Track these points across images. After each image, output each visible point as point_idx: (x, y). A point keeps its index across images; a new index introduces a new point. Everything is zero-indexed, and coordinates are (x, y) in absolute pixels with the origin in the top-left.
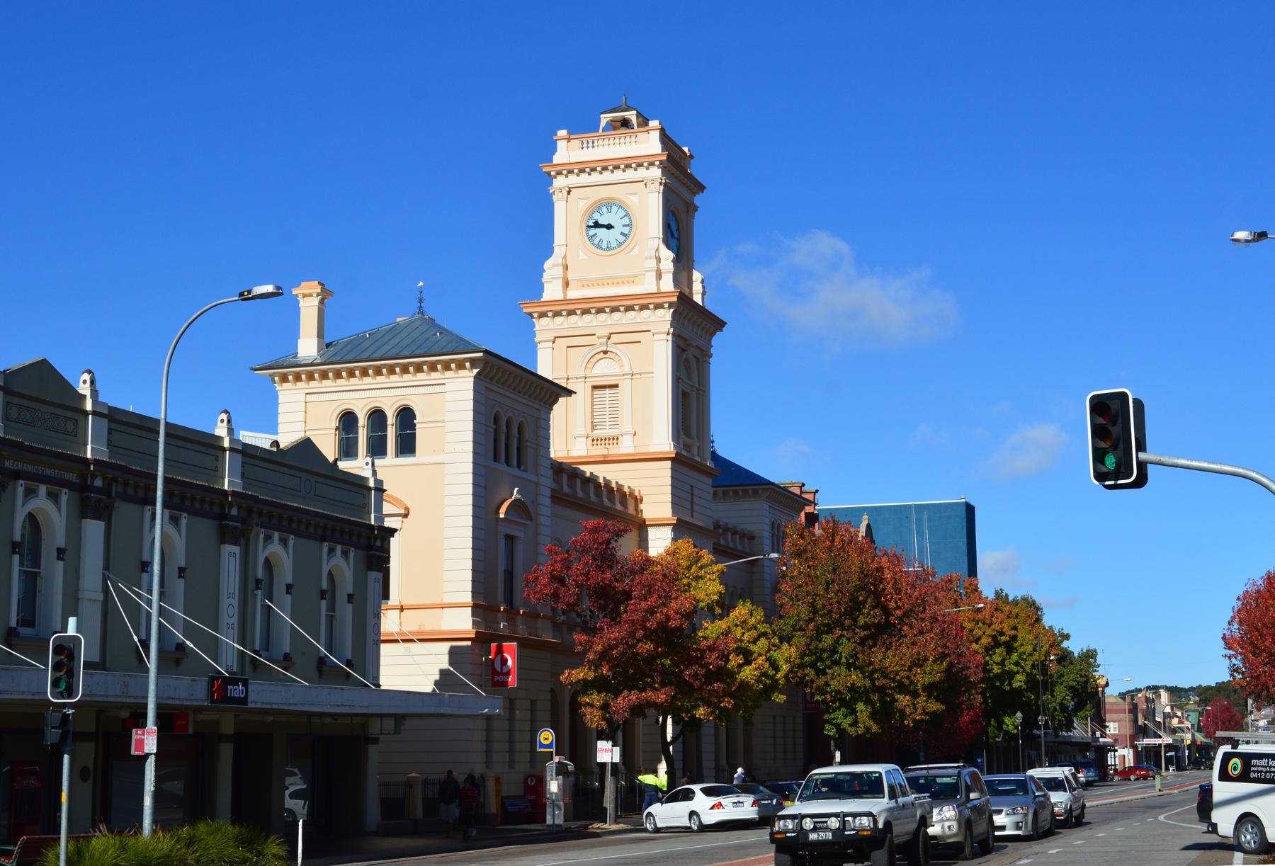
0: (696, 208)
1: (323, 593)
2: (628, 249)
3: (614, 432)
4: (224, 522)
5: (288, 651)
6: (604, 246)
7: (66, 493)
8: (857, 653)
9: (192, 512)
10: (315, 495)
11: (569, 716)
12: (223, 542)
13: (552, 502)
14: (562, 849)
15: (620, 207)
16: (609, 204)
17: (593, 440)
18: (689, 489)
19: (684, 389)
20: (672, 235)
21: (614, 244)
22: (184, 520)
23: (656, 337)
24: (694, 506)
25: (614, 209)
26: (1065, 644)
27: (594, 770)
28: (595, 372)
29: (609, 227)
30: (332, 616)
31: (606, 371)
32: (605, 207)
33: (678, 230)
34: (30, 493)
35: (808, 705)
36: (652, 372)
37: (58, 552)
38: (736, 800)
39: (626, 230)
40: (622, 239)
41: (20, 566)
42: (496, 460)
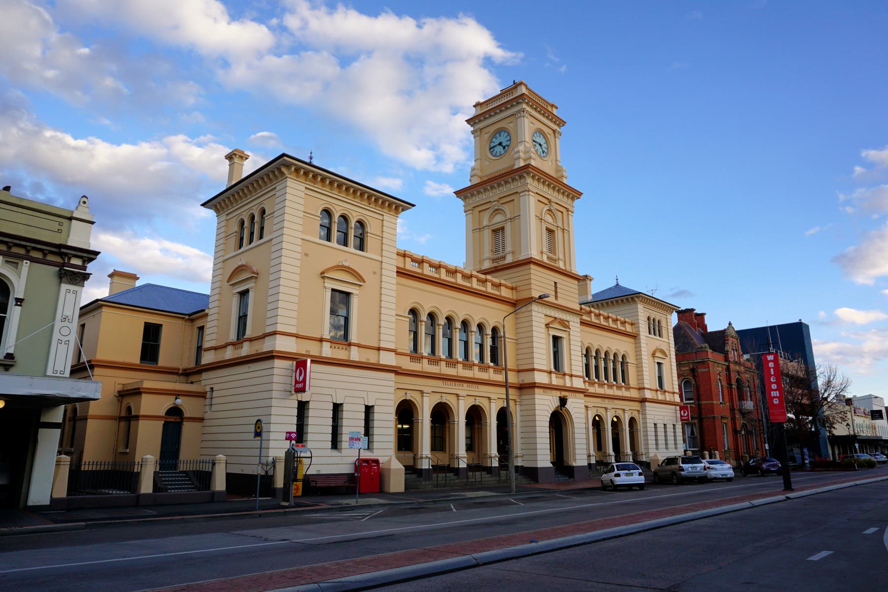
11: (629, 429)
13: (397, 275)
15: (505, 132)
17: (493, 261)
19: (547, 226)
23: (521, 194)
25: (502, 133)
27: (629, 454)
35: (683, 418)
38: (158, 462)
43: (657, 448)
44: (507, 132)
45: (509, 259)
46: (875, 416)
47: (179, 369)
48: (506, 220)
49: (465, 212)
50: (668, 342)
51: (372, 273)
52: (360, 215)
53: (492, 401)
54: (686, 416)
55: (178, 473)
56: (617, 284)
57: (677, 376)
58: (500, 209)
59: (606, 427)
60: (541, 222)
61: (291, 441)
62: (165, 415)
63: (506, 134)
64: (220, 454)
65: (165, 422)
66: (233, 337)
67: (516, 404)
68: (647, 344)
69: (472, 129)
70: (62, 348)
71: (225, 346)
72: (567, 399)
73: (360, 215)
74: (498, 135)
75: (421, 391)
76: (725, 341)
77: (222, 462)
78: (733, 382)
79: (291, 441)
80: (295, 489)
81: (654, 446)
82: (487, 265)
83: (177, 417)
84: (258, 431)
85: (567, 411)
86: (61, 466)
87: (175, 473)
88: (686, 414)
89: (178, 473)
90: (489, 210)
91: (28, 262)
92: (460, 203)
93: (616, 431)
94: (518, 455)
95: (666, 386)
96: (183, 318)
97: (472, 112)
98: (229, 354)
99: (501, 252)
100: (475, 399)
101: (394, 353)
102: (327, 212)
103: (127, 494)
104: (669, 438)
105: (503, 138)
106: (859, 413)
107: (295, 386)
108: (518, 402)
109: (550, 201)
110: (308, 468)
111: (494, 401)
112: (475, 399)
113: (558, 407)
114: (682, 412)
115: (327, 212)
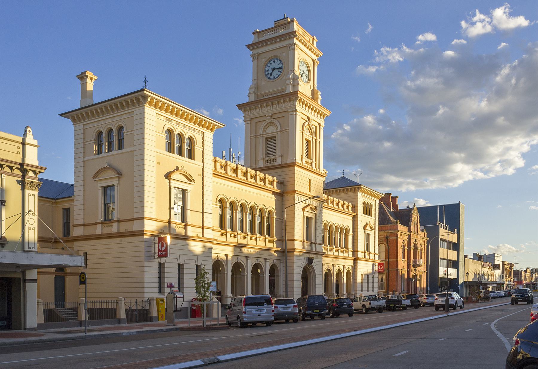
2: (281, 78)
3: (274, 157)
15: (278, 59)
16: (274, 59)
17: (266, 161)
18: (308, 180)
19: (307, 138)
21: (276, 76)
23: (290, 113)
24: (307, 200)
26: (514, 268)
27: (345, 294)
30: (24, 138)
31: (271, 131)
32: (272, 61)
43: (362, 291)
44: (280, 61)
45: (278, 162)
46: (495, 268)
47: (52, 239)
48: (277, 132)
49: (245, 122)
50: (374, 219)
51: (198, 175)
53: (249, 259)
54: (164, 251)
55: (65, 309)
57: (378, 240)
58: (273, 123)
59: (246, 273)
61: (171, 288)
62: (56, 271)
63: (279, 62)
65: (56, 276)
66: (101, 218)
67: (280, 263)
69: (251, 53)
70: (32, 232)
71: (96, 224)
72: (313, 260)
74: (272, 62)
75: (265, 258)
76: (410, 217)
77: (155, 300)
78: (412, 246)
79: (171, 288)
80: (161, 317)
81: (361, 289)
82: (261, 164)
83: (62, 273)
84: (83, 280)
85: (313, 267)
86: (39, 305)
87: (63, 309)
88: (381, 269)
89: (65, 309)
90: (265, 121)
92: (241, 113)
93: (273, 278)
94: (281, 295)
95: (372, 250)
96: (50, 201)
97: (252, 39)
98: (98, 230)
99: (272, 155)
100: (274, 261)
101: (212, 230)
102: (170, 132)
103: (74, 321)
104: (375, 284)
105: (277, 65)
106: (486, 266)
107: (158, 253)
108: (282, 261)
110: (182, 304)
111: (268, 261)
112: (257, 260)
113: (306, 265)
114: (379, 266)
115: (170, 132)
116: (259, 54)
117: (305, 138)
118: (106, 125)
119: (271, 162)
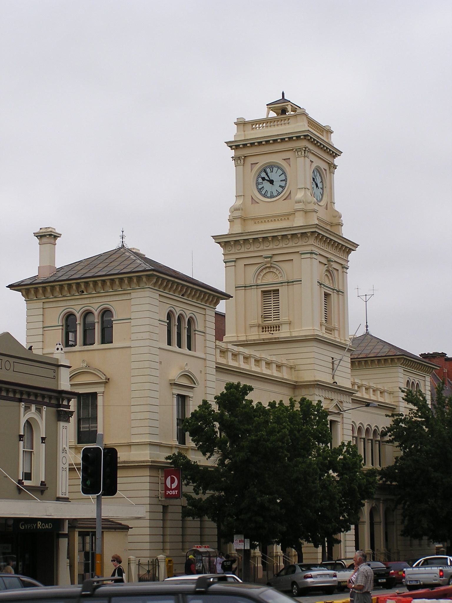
0: (335, 167)
1: (21, 437)
4: (59, 409)
5: (43, 480)
6: (269, 195)
7: (45, 408)
8: (283, 443)
9: (48, 405)
10: (13, 371)
12: (59, 420)
14: (279, 593)
15: (279, 168)
16: (272, 166)
17: (263, 328)
18: (331, 360)
20: (317, 186)
21: (275, 194)
22: (44, 409)
25: (275, 169)
28: (265, 281)
29: (271, 182)
33: (322, 182)
34: (27, 408)
36: (301, 281)
37: (42, 440)
39: (283, 184)
40: (280, 190)
41: (23, 448)
42: (169, 343)
44: (282, 170)
49: (225, 262)
52: (171, 307)
54: (175, 489)
56: (367, 334)
60: (321, 287)
64: (131, 555)
68: (161, 362)
73: (171, 307)
88: (174, 486)
91: (45, 407)
99: (272, 319)
109: (329, 261)
114: (169, 479)
116: (246, 156)
117: (324, 292)
118: (84, 305)
119: (271, 331)
